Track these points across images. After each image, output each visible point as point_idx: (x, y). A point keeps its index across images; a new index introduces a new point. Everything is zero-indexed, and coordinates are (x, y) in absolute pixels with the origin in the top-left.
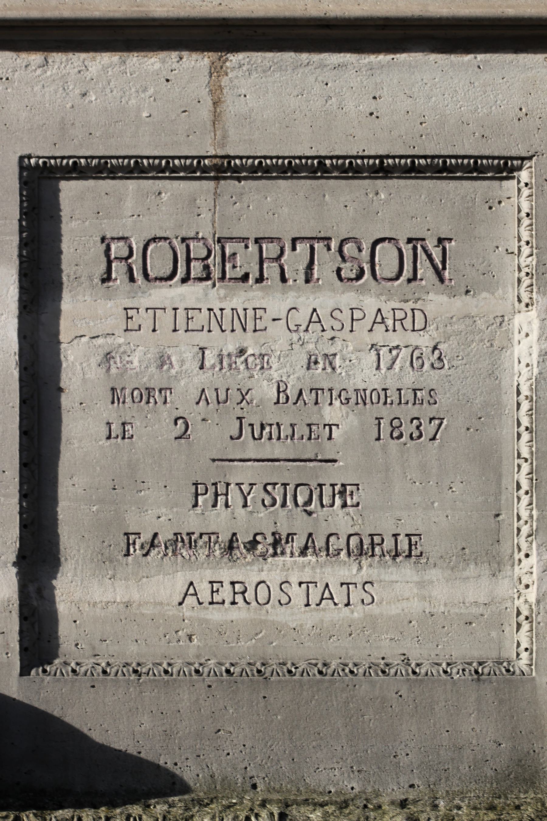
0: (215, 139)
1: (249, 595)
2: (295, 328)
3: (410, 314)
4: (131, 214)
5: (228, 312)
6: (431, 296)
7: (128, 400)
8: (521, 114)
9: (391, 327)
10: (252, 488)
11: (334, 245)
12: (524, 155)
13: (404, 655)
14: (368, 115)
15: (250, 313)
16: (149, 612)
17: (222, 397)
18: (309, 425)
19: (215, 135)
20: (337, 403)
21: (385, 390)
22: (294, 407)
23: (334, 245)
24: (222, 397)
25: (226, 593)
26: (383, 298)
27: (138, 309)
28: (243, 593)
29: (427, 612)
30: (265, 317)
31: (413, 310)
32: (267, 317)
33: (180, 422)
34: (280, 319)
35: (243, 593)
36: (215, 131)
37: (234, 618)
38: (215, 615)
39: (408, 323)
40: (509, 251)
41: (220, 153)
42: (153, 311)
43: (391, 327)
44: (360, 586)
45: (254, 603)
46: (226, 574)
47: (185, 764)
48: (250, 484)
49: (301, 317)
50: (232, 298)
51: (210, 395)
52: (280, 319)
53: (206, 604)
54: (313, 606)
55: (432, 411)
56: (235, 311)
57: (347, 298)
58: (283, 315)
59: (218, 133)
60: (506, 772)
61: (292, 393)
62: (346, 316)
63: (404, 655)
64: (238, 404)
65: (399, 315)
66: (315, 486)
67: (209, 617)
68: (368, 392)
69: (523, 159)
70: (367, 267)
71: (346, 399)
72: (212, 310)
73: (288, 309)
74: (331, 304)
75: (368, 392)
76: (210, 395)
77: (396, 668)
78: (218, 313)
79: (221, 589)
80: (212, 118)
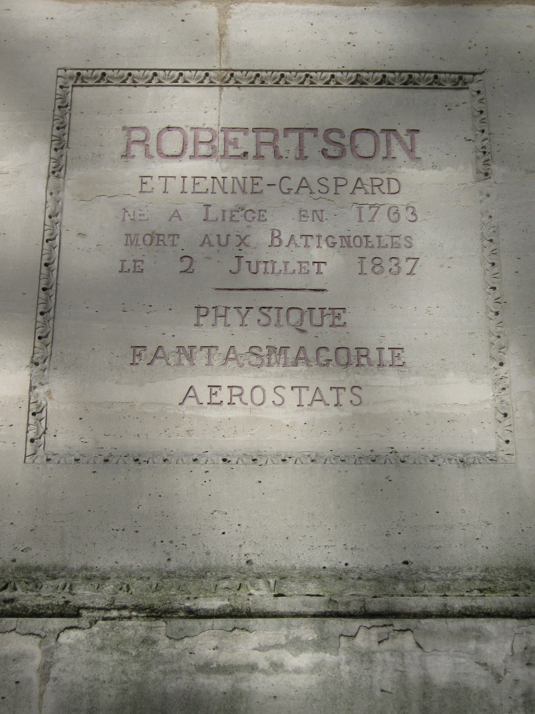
0: (220, 58)
1: (246, 397)
2: (287, 191)
3: (386, 182)
4: (149, 111)
5: (229, 180)
6: (403, 169)
7: (140, 242)
8: (472, 45)
9: (370, 191)
10: (248, 311)
11: (321, 133)
12: (476, 70)
13: (392, 448)
14: (346, 44)
15: (249, 180)
16: (151, 411)
17: (223, 241)
18: (300, 262)
19: (220, 56)
20: (324, 246)
21: (367, 237)
22: (287, 248)
23: (321, 133)
24: (223, 241)
25: (224, 395)
26: (362, 170)
27: (152, 177)
28: (240, 395)
29: (412, 412)
30: (261, 182)
31: (388, 179)
32: (262, 184)
33: (187, 261)
34: (274, 185)
35: (240, 395)
36: (220, 53)
37: (230, 416)
38: (213, 413)
39: (384, 188)
40: (468, 139)
41: (224, 67)
42: (164, 178)
43: (370, 191)
44: (348, 390)
45: (250, 404)
46: (225, 380)
47: (181, 543)
48: (247, 308)
49: (294, 183)
50: (145, 620)
51: (214, 239)
52: (274, 185)
53: (205, 404)
54: (306, 406)
55: (408, 253)
56: (235, 179)
57: (332, 170)
58: (277, 182)
59: (222, 54)
60: (497, 549)
61: (285, 238)
62: (331, 184)
63: (392, 448)
64: (237, 246)
65: (377, 182)
66: (306, 309)
67: (207, 415)
68: (352, 239)
69: (474, 74)
70: (348, 149)
71: (332, 243)
72: (216, 178)
73: (281, 177)
74: (318, 174)
75: (352, 239)
76: (214, 239)
77: (385, 458)
78: (221, 180)
79: (219, 392)
80: (218, 44)
